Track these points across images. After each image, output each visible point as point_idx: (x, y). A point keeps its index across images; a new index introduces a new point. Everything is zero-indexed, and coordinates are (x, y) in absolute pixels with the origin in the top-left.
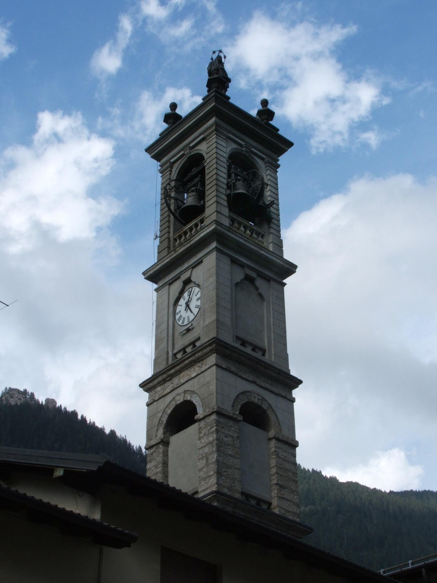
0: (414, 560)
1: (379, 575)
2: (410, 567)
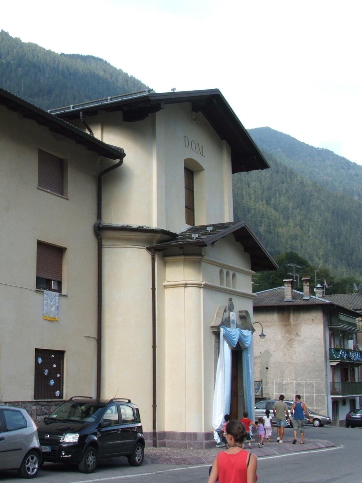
0: (75, 105)
1: (47, 113)
2: (71, 110)
